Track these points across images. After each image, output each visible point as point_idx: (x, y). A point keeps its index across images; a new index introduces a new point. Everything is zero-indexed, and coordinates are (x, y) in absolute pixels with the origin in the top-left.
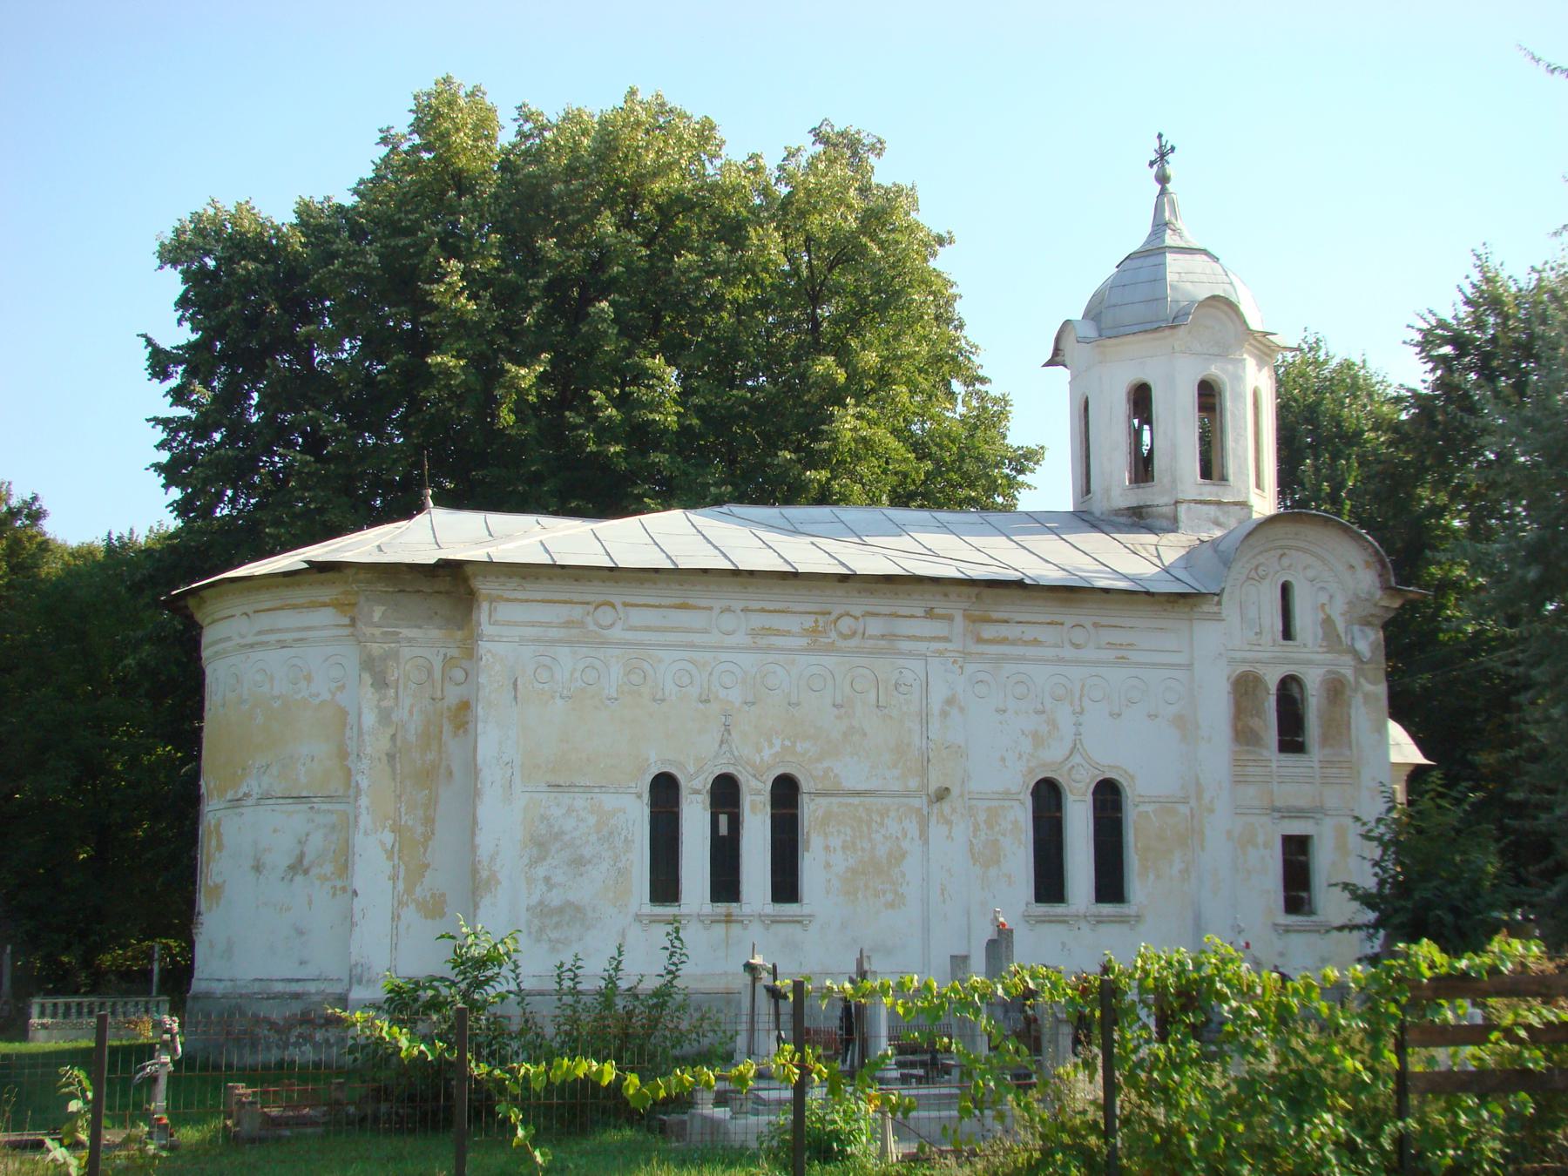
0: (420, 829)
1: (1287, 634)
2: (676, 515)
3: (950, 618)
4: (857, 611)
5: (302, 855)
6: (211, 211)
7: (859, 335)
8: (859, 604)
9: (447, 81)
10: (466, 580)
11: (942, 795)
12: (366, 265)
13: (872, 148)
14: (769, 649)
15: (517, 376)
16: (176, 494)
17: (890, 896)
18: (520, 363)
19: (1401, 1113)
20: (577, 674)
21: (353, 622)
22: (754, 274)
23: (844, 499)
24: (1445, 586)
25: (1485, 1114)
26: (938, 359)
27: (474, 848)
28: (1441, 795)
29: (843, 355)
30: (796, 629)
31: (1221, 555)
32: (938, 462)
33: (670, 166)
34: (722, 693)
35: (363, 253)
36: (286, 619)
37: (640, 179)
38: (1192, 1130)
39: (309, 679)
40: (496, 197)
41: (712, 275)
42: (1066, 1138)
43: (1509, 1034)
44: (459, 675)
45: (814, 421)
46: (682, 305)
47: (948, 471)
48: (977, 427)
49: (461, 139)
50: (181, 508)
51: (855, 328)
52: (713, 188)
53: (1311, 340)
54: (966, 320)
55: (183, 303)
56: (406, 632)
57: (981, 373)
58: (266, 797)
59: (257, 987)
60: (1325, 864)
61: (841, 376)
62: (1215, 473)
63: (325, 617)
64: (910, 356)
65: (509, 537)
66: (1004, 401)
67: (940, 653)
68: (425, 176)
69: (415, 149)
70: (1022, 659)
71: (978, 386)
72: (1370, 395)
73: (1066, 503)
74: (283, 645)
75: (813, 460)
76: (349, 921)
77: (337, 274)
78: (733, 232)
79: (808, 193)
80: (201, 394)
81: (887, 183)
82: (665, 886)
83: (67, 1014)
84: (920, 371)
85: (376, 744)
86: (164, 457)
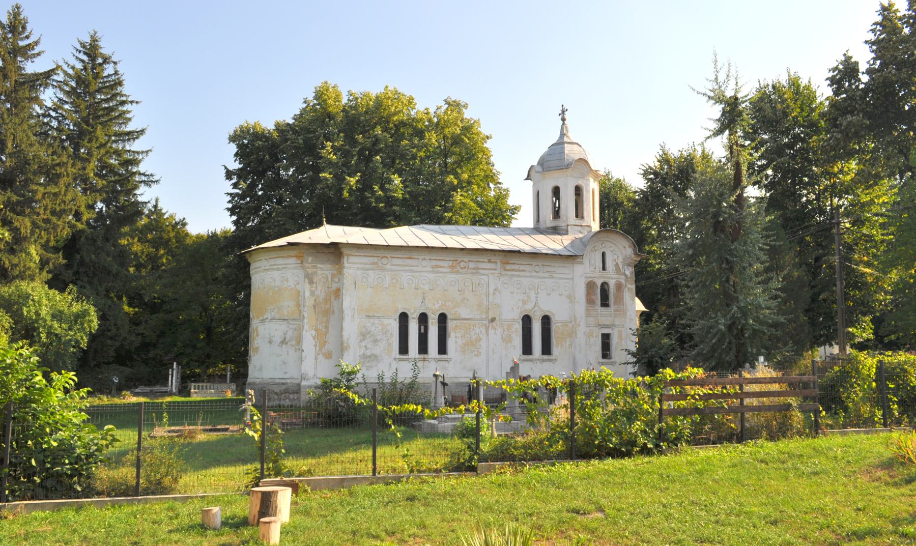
0: (324, 330)
1: (604, 268)
2: (406, 227)
3: (496, 263)
4: (466, 260)
5: (285, 338)
6: (246, 125)
7: (461, 168)
9: (326, 83)
10: (339, 249)
11: (493, 320)
13: (464, 106)
14: (438, 272)
15: (349, 181)
16: (234, 218)
17: (476, 353)
18: (351, 177)
21: (302, 262)
23: (457, 223)
24: (649, 253)
26: (487, 177)
27: (342, 336)
28: (657, 321)
29: (457, 176)
30: (446, 266)
31: (584, 243)
32: (486, 210)
33: (400, 112)
34: (422, 286)
36: (280, 261)
39: (287, 280)
40: (341, 121)
41: (413, 148)
43: (693, 397)
44: (336, 280)
45: (448, 198)
46: (403, 157)
50: (235, 223)
51: (460, 166)
52: (414, 119)
53: (607, 172)
55: (236, 155)
56: (319, 266)
57: (500, 181)
58: (273, 319)
59: (270, 381)
61: (456, 182)
63: (292, 261)
64: (478, 176)
66: (507, 190)
67: (493, 274)
68: (319, 114)
69: (314, 105)
70: (519, 276)
72: (626, 190)
73: (530, 224)
74: (278, 269)
75: (446, 210)
77: (289, 146)
78: (420, 134)
79: (445, 121)
80: (243, 185)
81: (469, 118)
82: (404, 349)
83: (202, 389)
85: (310, 302)
86: (230, 206)
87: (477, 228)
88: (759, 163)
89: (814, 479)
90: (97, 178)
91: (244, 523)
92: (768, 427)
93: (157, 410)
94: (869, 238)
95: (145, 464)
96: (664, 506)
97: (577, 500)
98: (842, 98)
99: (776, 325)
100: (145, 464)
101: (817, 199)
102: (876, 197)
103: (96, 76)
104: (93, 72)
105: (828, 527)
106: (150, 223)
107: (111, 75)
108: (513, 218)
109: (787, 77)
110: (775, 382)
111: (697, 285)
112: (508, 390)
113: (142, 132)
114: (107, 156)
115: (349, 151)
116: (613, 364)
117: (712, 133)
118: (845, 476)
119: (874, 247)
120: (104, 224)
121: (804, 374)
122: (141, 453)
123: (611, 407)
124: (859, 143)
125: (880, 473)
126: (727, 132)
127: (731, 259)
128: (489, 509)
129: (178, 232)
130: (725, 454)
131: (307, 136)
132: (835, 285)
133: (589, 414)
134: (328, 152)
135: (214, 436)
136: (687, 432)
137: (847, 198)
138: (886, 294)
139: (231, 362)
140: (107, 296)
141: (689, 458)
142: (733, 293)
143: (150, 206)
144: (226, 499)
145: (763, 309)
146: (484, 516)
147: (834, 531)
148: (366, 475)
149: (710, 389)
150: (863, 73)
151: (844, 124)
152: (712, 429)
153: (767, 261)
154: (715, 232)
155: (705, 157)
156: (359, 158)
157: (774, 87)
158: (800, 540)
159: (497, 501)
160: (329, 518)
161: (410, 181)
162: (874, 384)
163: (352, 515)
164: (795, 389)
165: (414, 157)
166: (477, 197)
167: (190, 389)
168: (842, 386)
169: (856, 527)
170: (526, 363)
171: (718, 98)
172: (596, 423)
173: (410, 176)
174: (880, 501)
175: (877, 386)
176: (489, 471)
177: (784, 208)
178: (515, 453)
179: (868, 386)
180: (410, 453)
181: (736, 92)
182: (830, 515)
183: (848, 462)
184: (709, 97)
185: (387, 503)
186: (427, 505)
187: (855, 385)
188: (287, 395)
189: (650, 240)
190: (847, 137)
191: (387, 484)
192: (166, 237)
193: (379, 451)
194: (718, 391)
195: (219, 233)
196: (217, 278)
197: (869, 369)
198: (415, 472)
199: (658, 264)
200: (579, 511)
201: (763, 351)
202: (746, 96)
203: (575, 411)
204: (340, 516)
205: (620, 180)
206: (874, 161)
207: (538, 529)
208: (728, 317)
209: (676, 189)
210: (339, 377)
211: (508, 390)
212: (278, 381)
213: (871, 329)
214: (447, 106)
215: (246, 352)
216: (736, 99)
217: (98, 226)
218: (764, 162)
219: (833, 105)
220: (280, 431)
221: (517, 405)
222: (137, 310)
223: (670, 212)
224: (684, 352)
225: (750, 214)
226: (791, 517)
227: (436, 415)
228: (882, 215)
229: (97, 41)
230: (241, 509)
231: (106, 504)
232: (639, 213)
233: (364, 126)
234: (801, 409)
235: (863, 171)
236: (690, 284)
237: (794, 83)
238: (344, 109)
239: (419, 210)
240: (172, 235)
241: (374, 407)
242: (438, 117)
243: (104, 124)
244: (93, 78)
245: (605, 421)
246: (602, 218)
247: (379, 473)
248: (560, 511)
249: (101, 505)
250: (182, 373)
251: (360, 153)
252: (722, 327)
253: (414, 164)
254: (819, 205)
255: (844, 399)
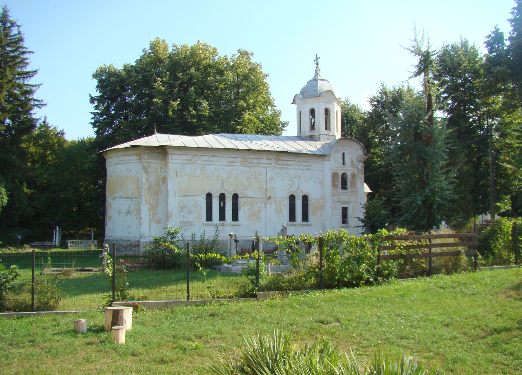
1: (344, 164)
2: (211, 135)
3: (271, 159)
4: (251, 157)
5: (129, 210)
6: (104, 67)
7: (249, 96)
8: (252, 156)
9: (158, 38)
11: (270, 198)
12: (139, 79)
13: (251, 55)
14: (232, 166)
16: (96, 129)
17: (258, 220)
18: (174, 101)
19: (378, 264)
20: (190, 171)
21: (140, 159)
22: (225, 82)
23: (245, 133)
24: (374, 154)
25: (394, 264)
26: (266, 102)
27: (167, 209)
28: (378, 199)
29: (246, 101)
30: (238, 161)
31: (330, 146)
32: (266, 124)
33: (207, 58)
34: (222, 175)
35: (138, 76)
36: (126, 158)
37: (201, 60)
38: (337, 268)
39: (131, 171)
40: (168, 64)
41: (216, 82)
42: (312, 270)
43: (399, 247)
44: (164, 171)
45: (239, 115)
46: (209, 88)
47: (267, 126)
48: (274, 117)
49: (160, 51)
50: (97, 132)
52: (216, 63)
53: (347, 100)
54: (271, 93)
55: (97, 87)
56: (152, 161)
57: (274, 105)
58: (121, 197)
59: (120, 238)
60: (350, 213)
62: (328, 128)
63: (134, 157)
64: (260, 101)
65: (174, 140)
67: (269, 167)
69: (150, 53)
70: (287, 169)
71: (274, 108)
72: (359, 112)
73: (295, 134)
74: (125, 164)
75: (238, 124)
76: (140, 224)
77: (133, 81)
78: (221, 72)
79: (238, 64)
80: (102, 107)
81: (254, 62)
82: (209, 218)
84: (262, 104)
85: (146, 186)
86: (93, 121)
87: (259, 136)
88: (443, 96)
89: (472, 297)
90: (6, 103)
91: (102, 329)
92: (446, 266)
93: (45, 256)
94: (510, 146)
95: (37, 291)
96: (379, 317)
97: (323, 315)
98: (493, 55)
99: (453, 201)
100: (37, 291)
101: (479, 120)
102: (514, 119)
103: (6, 35)
104: (4, 33)
105: (479, 327)
106: (41, 134)
107: (16, 34)
108: (284, 130)
109: (460, 41)
110: (451, 237)
111: (403, 175)
112: (279, 244)
113: (36, 72)
114: (13, 88)
115: (172, 84)
116: (349, 227)
117: (413, 75)
118: (491, 295)
119: (513, 151)
120: (11, 134)
121: (470, 232)
122: (34, 284)
123: (347, 255)
124: (504, 85)
125: (512, 293)
126: (423, 74)
127: (425, 157)
128: (264, 321)
129: (59, 139)
130: (419, 284)
131: (145, 74)
132: (489, 176)
133: (332, 259)
134: (159, 84)
135: (83, 275)
136: (395, 270)
137: (497, 120)
138: (519, 181)
139: (94, 226)
140: (13, 181)
141: (396, 287)
142: (426, 180)
143: (41, 121)
144: (90, 314)
145: (445, 190)
146: (261, 326)
147: (482, 329)
148: (183, 300)
149: (411, 242)
150: (506, 40)
151: (495, 72)
152: (411, 268)
153: (448, 160)
154: (415, 140)
155: (409, 91)
156: (180, 89)
157: (452, 47)
158: (462, 336)
159: (270, 316)
160: (158, 327)
161: (214, 104)
162: (510, 238)
163: (173, 325)
164: (463, 241)
165: (217, 88)
166: (259, 116)
167: (68, 244)
168: (492, 239)
169: (496, 326)
170: (291, 227)
171: (417, 52)
172: (337, 265)
173: (214, 101)
174: (511, 309)
175: (512, 239)
176: (265, 297)
177: (459, 125)
178: (283, 285)
179: (507, 239)
180: (212, 285)
181: (428, 48)
182: (481, 319)
183: (494, 286)
184: (411, 51)
185: (197, 318)
186: (223, 319)
187: (500, 239)
188: (131, 248)
189: (374, 145)
190: (497, 81)
191: (197, 306)
192: (51, 142)
193: (192, 285)
194: (415, 243)
195: (86, 139)
196: (85, 170)
197: (508, 228)
198: (216, 298)
199: (380, 161)
200: (324, 322)
201: (444, 217)
202: (434, 51)
203: (323, 258)
204: (165, 326)
205: (354, 105)
206: (512, 97)
207: (297, 334)
208: (423, 195)
209: (391, 112)
210: (165, 235)
211: (279, 244)
212: (125, 239)
213: (510, 203)
214: (239, 54)
215: (104, 219)
216: (428, 53)
217: (7, 135)
218: (446, 95)
219: (488, 59)
220: (125, 270)
221: (285, 254)
222: (32, 191)
223: (387, 127)
224: (395, 219)
225: (438, 128)
226: (457, 321)
227: (230, 261)
228: (517, 131)
229: (7, 12)
230: (100, 321)
231: (13, 316)
232: (367, 127)
233: (183, 67)
234: (468, 255)
235: (506, 102)
236: (400, 174)
237: (464, 45)
238: (170, 56)
239: (220, 124)
240: (55, 141)
241: (188, 255)
242: (233, 61)
243: (11, 67)
244: (5, 37)
245: (343, 264)
246: (342, 130)
247: (192, 299)
248: (311, 322)
249: (9, 316)
250: (62, 234)
251: (181, 85)
252: (419, 202)
253: (216, 93)
254: (480, 124)
255: (492, 248)
